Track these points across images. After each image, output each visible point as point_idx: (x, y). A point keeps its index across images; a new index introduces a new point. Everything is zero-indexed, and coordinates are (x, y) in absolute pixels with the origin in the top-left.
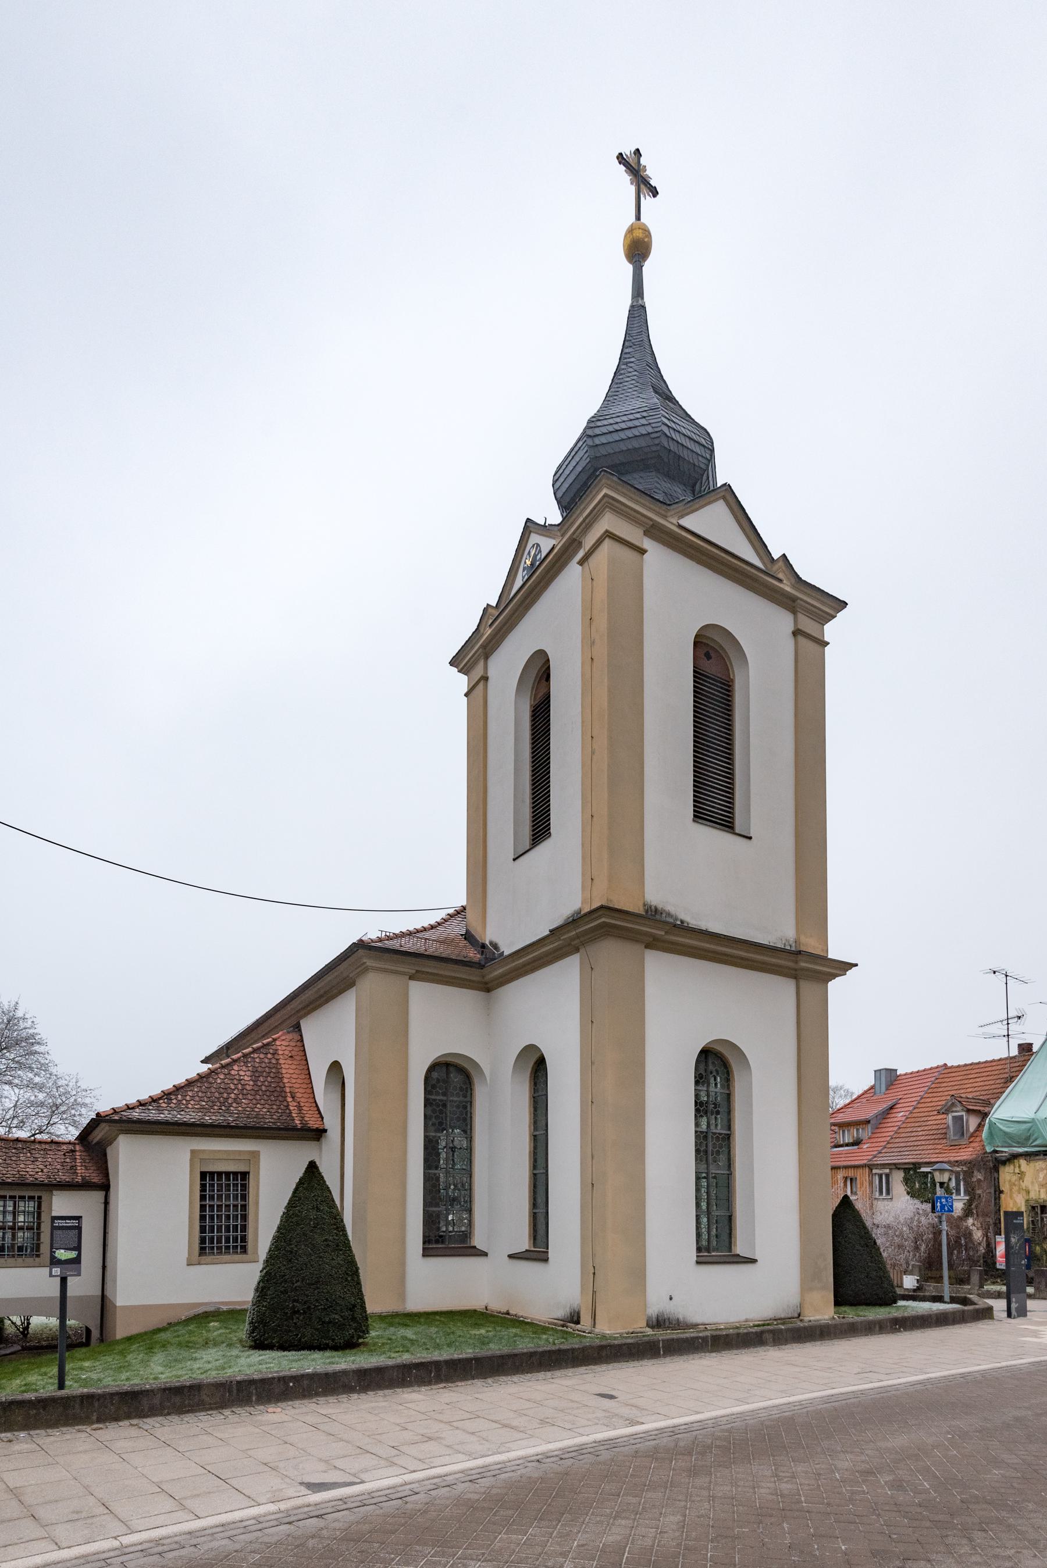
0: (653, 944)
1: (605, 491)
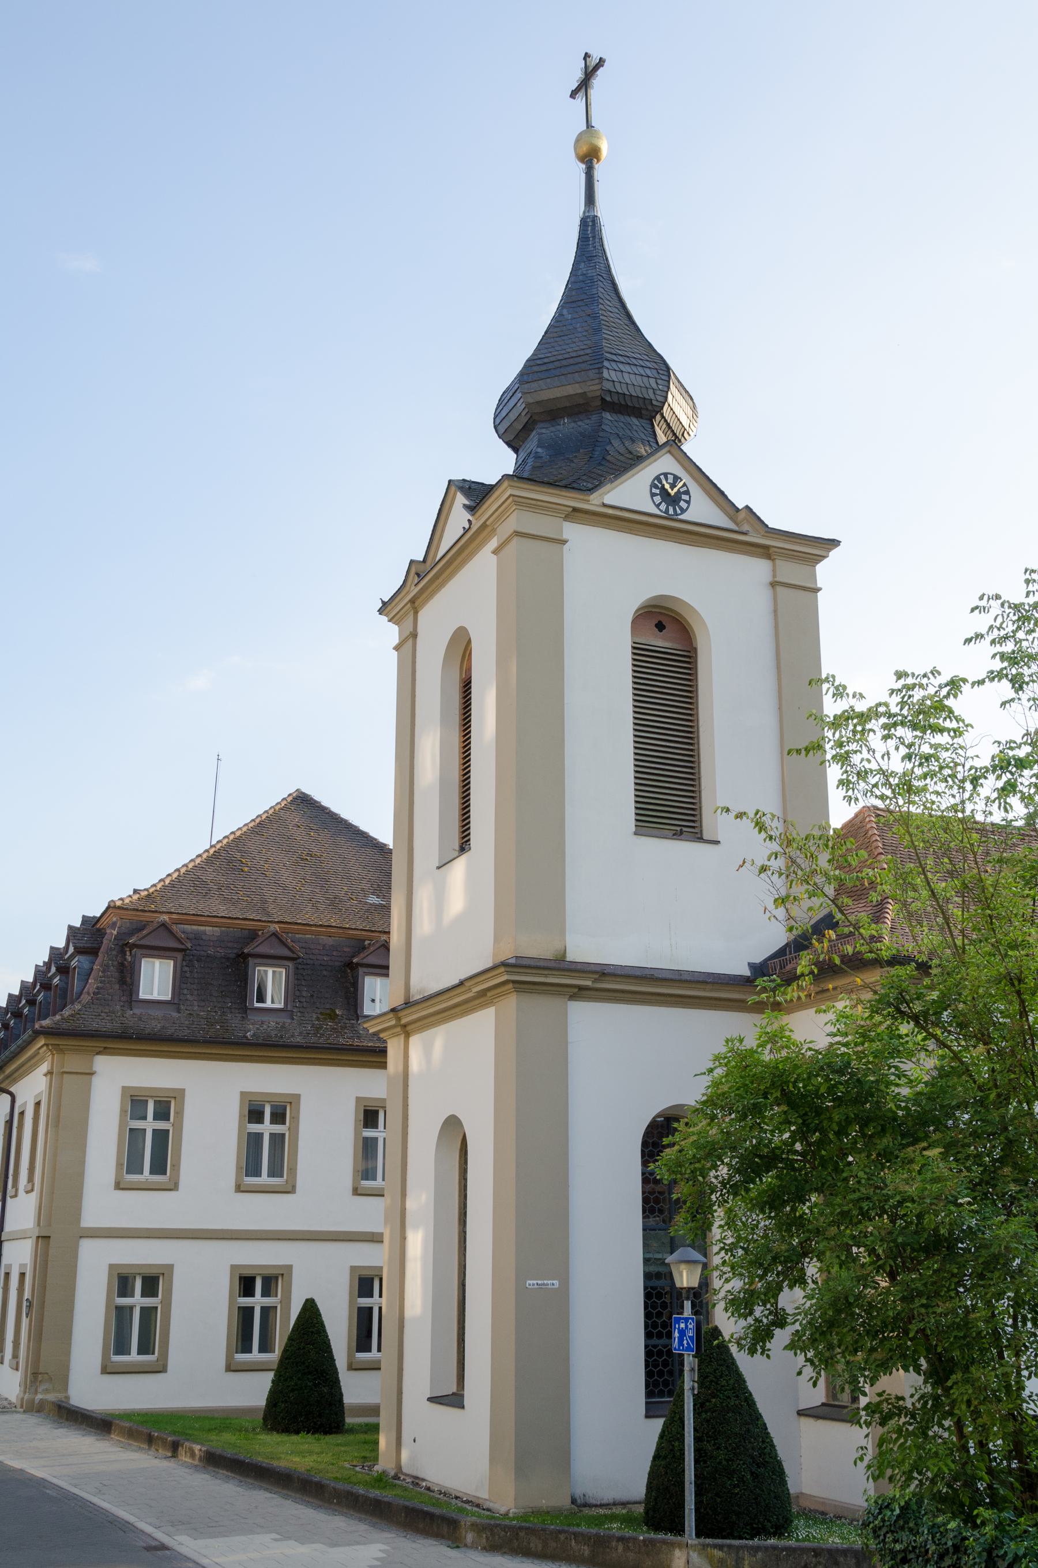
0: (579, 993)
1: (509, 492)
